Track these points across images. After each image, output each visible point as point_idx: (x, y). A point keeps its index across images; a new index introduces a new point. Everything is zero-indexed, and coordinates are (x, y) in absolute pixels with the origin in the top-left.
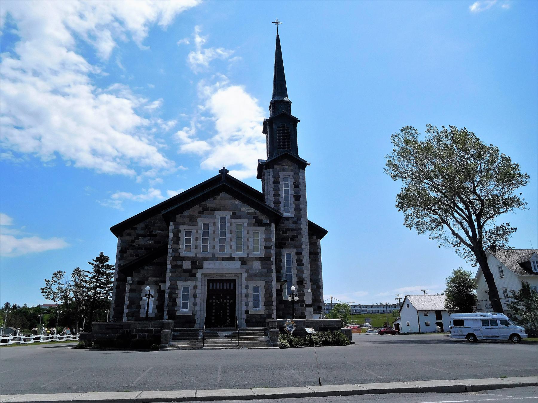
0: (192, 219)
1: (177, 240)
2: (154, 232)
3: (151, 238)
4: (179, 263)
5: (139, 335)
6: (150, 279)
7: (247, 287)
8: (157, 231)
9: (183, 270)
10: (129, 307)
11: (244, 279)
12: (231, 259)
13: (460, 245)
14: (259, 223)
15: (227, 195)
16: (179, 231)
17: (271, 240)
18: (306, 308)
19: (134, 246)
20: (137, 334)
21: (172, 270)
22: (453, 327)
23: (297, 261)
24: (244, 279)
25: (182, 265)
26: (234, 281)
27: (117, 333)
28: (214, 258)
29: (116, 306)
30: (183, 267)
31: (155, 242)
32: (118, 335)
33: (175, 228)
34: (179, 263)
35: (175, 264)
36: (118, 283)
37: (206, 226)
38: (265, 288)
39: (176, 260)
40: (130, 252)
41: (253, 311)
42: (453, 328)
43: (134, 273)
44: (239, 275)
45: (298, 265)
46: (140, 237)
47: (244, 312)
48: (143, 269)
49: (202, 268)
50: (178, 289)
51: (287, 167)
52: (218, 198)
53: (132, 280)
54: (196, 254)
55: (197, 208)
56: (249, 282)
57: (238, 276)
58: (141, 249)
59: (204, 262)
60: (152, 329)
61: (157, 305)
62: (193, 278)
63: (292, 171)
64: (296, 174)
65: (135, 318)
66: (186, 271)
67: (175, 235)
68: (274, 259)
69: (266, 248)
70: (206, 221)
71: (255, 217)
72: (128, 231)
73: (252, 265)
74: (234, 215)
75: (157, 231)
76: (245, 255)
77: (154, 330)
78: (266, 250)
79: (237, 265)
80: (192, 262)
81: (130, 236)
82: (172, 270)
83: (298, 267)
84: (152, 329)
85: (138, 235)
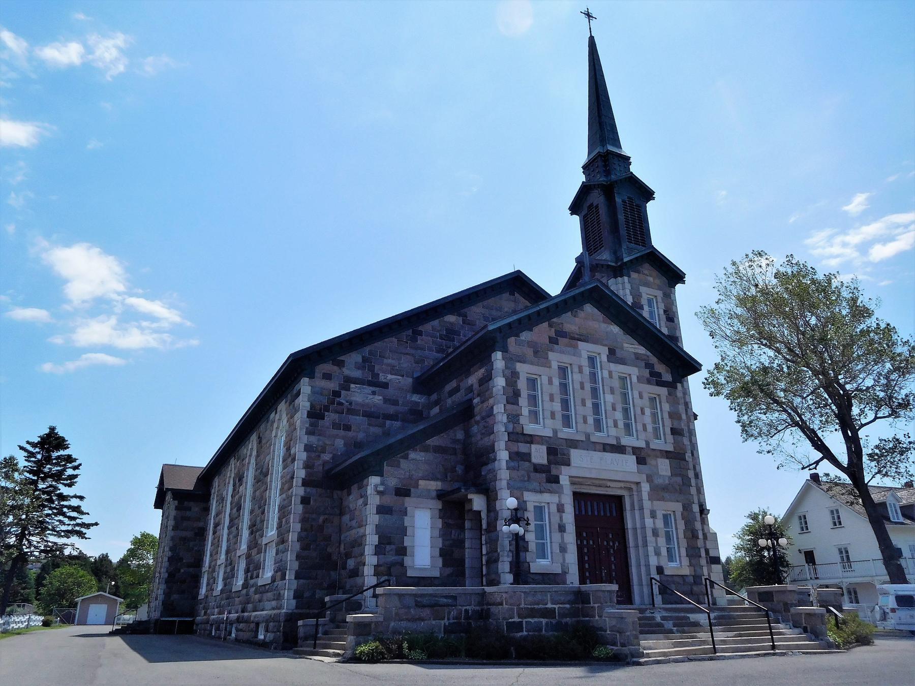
0: (538, 351)
1: (513, 397)
2: (382, 378)
3: (377, 389)
4: (523, 448)
5: (526, 622)
7: (653, 515)
8: (390, 377)
12: (619, 449)
13: (816, 466)
19: (340, 404)
20: (522, 621)
22: (898, 609)
25: (529, 454)
27: (443, 619)
28: (588, 445)
29: (304, 548)
31: (386, 400)
32: (447, 624)
33: (507, 367)
34: (523, 448)
35: (517, 450)
37: (563, 371)
38: (683, 519)
39: (518, 441)
41: (671, 568)
42: (897, 611)
44: (634, 487)
46: (352, 386)
48: (406, 457)
49: (569, 465)
51: (651, 279)
52: (581, 314)
53: (382, 484)
54: (555, 432)
60: (554, 606)
61: (440, 549)
63: (659, 288)
65: (394, 578)
66: (537, 468)
68: (689, 457)
69: (674, 431)
70: (566, 359)
71: (649, 366)
72: (327, 367)
73: (657, 466)
76: (642, 444)
77: (559, 608)
78: (676, 436)
79: (628, 463)
81: (331, 379)
82: (512, 464)
84: (554, 606)
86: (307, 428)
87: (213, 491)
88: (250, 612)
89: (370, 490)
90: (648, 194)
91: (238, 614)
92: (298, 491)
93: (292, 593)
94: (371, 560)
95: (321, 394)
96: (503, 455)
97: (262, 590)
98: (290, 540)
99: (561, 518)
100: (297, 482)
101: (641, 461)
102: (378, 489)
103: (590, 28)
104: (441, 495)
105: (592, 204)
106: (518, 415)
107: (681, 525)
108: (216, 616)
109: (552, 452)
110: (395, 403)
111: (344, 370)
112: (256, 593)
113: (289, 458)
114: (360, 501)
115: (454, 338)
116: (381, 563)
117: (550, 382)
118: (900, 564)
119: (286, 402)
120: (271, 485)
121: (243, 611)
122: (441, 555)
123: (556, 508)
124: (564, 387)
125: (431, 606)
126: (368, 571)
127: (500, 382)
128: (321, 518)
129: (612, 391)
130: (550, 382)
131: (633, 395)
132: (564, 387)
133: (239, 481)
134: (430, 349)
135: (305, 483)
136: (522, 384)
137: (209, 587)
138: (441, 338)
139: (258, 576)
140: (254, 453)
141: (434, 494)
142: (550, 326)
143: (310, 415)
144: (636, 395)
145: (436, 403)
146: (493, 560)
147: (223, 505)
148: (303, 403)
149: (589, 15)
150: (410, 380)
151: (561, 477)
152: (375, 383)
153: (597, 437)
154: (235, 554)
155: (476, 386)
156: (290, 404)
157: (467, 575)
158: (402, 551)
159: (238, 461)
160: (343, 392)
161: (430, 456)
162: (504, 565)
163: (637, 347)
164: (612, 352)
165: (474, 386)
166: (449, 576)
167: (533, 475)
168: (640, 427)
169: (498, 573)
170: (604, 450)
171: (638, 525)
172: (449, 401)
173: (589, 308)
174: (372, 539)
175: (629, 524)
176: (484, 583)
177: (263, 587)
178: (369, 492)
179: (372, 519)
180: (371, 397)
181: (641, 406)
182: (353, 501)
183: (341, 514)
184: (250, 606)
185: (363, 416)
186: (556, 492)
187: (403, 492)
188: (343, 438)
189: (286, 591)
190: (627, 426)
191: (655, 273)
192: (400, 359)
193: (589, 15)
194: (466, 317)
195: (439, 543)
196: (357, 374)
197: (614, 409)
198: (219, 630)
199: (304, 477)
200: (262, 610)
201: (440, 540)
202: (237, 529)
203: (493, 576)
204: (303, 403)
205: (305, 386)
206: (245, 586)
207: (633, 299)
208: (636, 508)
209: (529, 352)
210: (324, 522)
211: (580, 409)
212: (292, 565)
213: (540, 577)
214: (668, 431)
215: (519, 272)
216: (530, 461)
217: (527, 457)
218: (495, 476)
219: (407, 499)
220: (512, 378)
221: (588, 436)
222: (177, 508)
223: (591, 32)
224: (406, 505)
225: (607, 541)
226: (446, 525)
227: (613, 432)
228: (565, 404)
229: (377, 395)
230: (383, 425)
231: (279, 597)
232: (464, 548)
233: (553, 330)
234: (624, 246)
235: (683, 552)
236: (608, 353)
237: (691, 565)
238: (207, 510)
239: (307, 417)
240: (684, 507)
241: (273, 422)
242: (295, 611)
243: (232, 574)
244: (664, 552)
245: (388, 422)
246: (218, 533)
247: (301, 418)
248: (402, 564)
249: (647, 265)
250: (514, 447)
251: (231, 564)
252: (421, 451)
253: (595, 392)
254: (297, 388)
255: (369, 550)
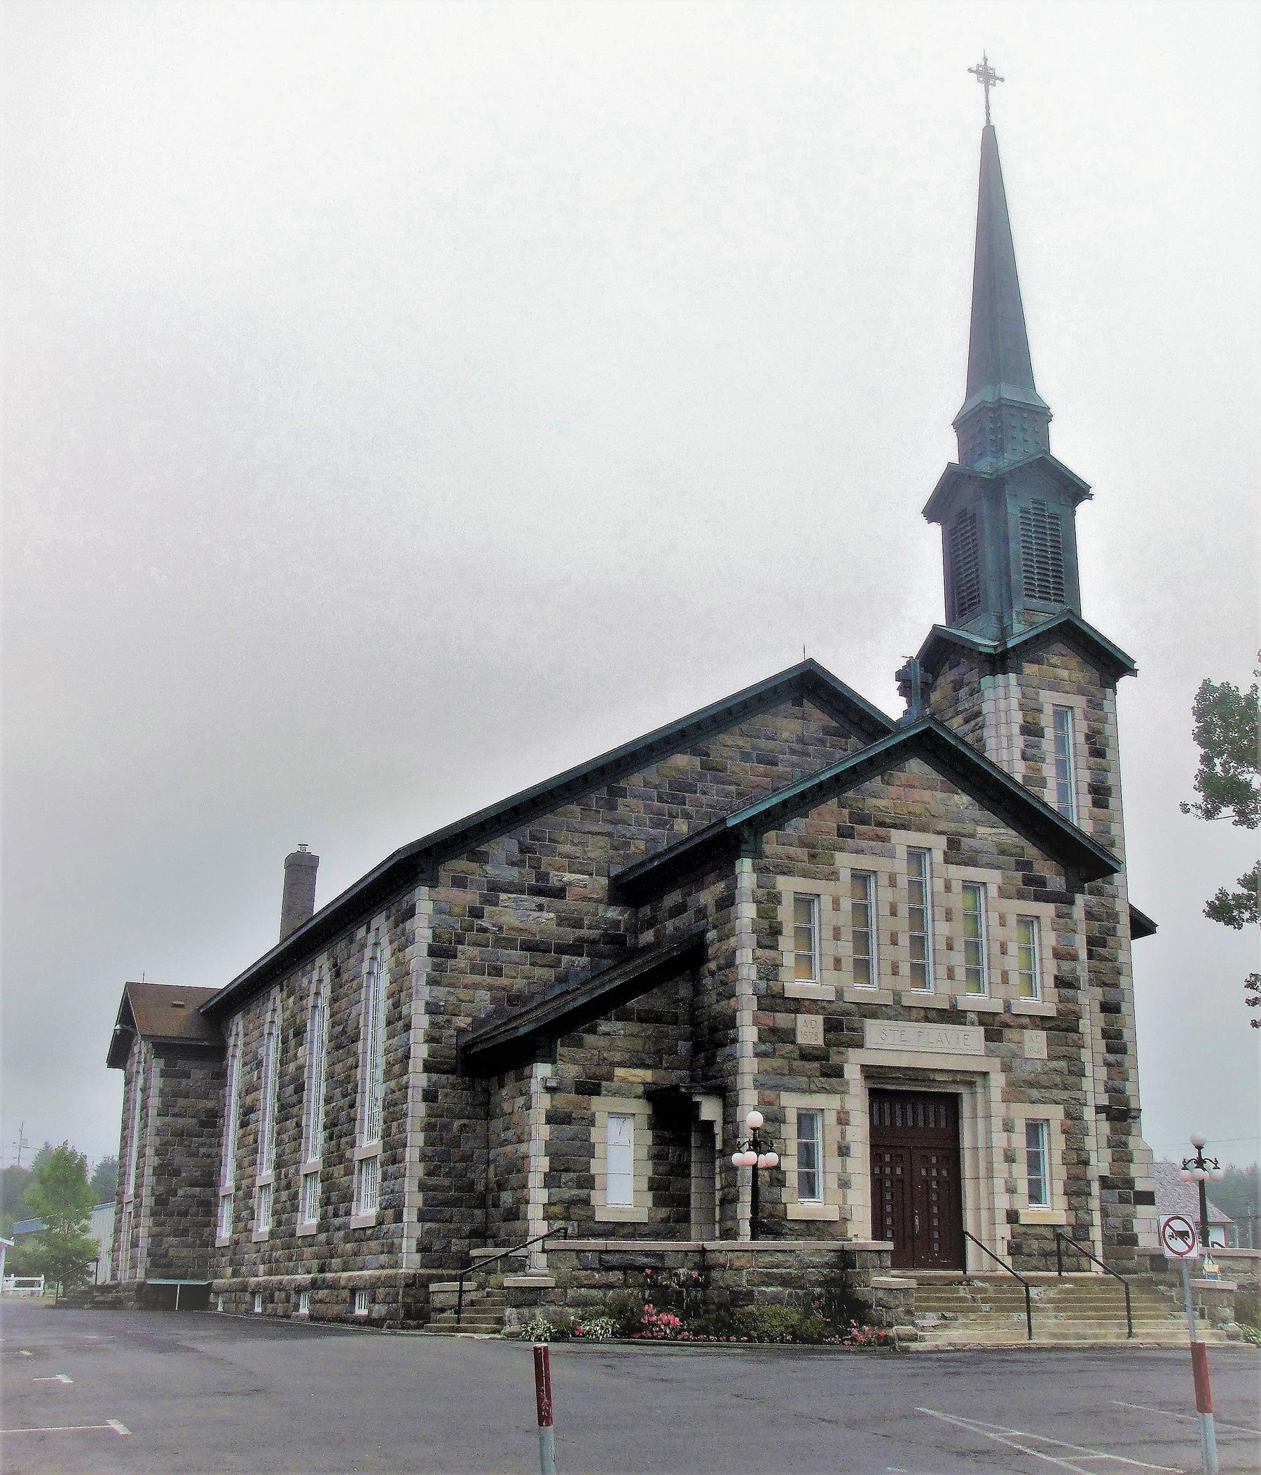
1: (769, 934)
4: (782, 1020)
6: (620, 1072)
7: (1008, 1127)
8: (568, 877)
9: (798, 1052)
10: (550, 1180)
11: (996, 1094)
12: (952, 1015)
14: (1035, 888)
15: (927, 769)
16: (775, 898)
17: (1074, 958)
18: (1138, 1206)
21: (763, 1047)
23: (1105, 1034)
24: (996, 1094)
25: (793, 1031)
26: (953, 1102)
28: (899, 1011)
30: (800, 1040)
31: (561, 921)
34: (782, 1020)
36: (429, 1081)
37: (861, 878)
40: (468, 953)
41: (1030, 1214)
43: (561, 1050)
45: (1110, 1050)
46: (503, 896)
47: (1001, 1217)
49: (861, 1046)
50: (784, 1122)
51: (1065, 674)
52: (900, 776)
53: (555, 1074)
54: (840, 994)
55: (828, 816)
56: (1012, 1105)
57: (971, 1084)
58: (509, 943)
59: (868, 1022)
62: (833, 1080)
63: (1081, 691)
64: (1096, 705)
66: (807, 1055)
67: (761, 914)
69: (1061, 982)
71: (1024, 865)
72: (461, 865)
74: (956, 852)
75: (568, 877)
76: (997, 1006)
80: (826, 1021)
82: (763, 1047)
83: (1111, 1058)
85: (495, 888)
86: (428, 975)
87: (231, 1041)
88: (336, 1272)
89: (535, 1086)
90: (1077, 491)
91: (311, 1275)
92: (418, 1079)
93: (414, 1243)
94: (538, 1195)
95: (450, 914)
96: (748, 1034)
97: (360, 1236)
98: (407, 1159)
99: (843, 1133)
100: (416, 1064)
101: (994, 1034)
102: (548, 1084)
103: (988, 107)
104: (652, 1095)
105: (964, 512)
106: (776, 966)
107: (1059, 1142)
108: (264, 1278)
109: (833, 1026)
110: (578, 924)
111: (488, 868)
112: (346, 1240)
113: (398, 1022)
114: (521, 1101)
115: (684, 797)
116: (554, 1199)
117: (836, 905)
118: (83, 1308)
119: (388, 918)
120: (364, 1059)
121: (322, 1270)
122: (650, 1189)
123: (835, 1119)
124: (861, 911)
125: (624, 1268)
126: (535, 1212)
127: (747, 911)
128: (457, 1124)
129: (949, 916)
130: (836, 905)
131: (989, 920)
132: (861, 911)
133: (296, 1035)
134: (639, 823)
135: (428, 1068)
136: (786, 913)
137: (241, 1225)
138: (661, 800)
139: (348, 1213)
140: (326, 991)
141: (640, 1090)
142: (842, 805)
143: (432, 952)
144: (994, 918)
145: (650, 923)
146: (729, 1201)
147: (259, 1073)
148: (422, 929)
149: (986, 75)
150: (604, 881)
151: (847, 1068)
152: (547, 891)
153: (916, 996)
154: (297, 1170)
155: (711, 909)
156: (396, 926)
157: (693, 1221)
158: (588, 1182)
159: (288, 997)
160: (488, 909)
161: (633, 1027)
162: (744, 1211)
163: (1002, 831)
164: (953, 844)
165: (709, 910)
166: (665, 1220)
167: (798, 1064)
168: (997, 977)
169: (736, 1218)
170: (927, 1019)
171: (981, 1144)
172: (670, 925)
173: (916, 767)
174: (540, 1164)
175: (966, 1141)
176: (717, 1234)
177: (361, 1231)
178: (533, 1089)
179: (541, 1132)
180: (536, 914)
181: (1002, 940)
182: (507, 1098)
183: (489, 1116)
184: (336, 1262)
185: (522, 950)
186: (835, 1092)
187: (589, 1088)
188: (490, 988)
189: (405, 1239)
190: (974, 975)
191: (1074, 661)
192: (584, 844)
193: (986, 75)
194: (707, 755)
195: (648, 1169)
196: (513, 874)
197: (950, 947)
198: (272, 1302)
199: (426, 1056)
200: (361, 1269)
201: (650, 1164)
202: (298, 1125)
203: (729, 1224)
204: (422, 929)
205: (424, 900)
206: (322, 1227)
207: (1025, 716)
208: (980, 1114)
209: (802, 853)
210: (462, 1130)
211: (888, 951)
212: (413, 1200)
213: (803, 1226)
214: (1050, 981)
215: (811, 661)
216: (793, 1042)
217: (787, 1036)
218: (736, 1067)
219: (595, 1098)
220: (768, 902)
221: (897, 996)
222: (164, 1074)
223: (988, 114)
224: (593, 1109)
225: (927, 1169)
226: (658, 1141)
227: (945, 987)
228: (862, 940)
229: (545, 912)
230: (555, 965)
231: (392, 1249)
232: (689, 1175)
233: (846, 811)
234: (1018, 607)
235: (1059, 1187)
236: (945, 847)
237: (1071, 1208)
238: (221, 1076)
239: (428, 956)
240: (1068, 1115)
241: (364, 946)
242: (421, 1271)
243: (292, 1205)
244: (1023, 1187)
245: (565, 958)
246: (252, 1126)
247: (419, 958)
248: (586, 1202)
249: (1059, 647)
250: (768, 1019)
251: (288, 1187)
252: (618, 1019)
253: (917, 915)
254: (407, 899)
255: (535, 1180)
